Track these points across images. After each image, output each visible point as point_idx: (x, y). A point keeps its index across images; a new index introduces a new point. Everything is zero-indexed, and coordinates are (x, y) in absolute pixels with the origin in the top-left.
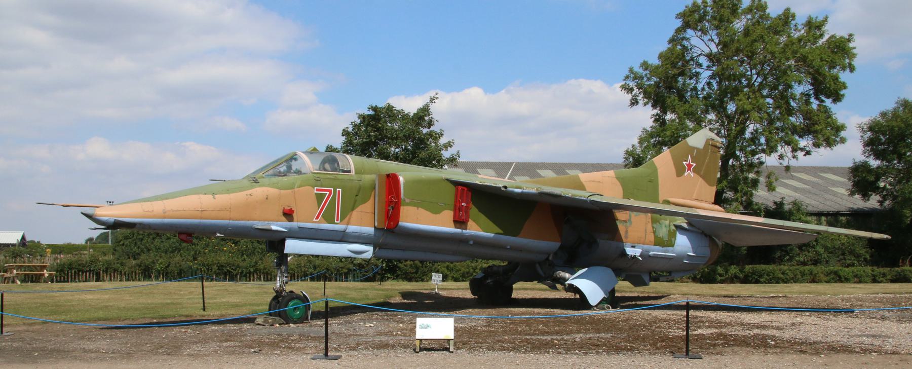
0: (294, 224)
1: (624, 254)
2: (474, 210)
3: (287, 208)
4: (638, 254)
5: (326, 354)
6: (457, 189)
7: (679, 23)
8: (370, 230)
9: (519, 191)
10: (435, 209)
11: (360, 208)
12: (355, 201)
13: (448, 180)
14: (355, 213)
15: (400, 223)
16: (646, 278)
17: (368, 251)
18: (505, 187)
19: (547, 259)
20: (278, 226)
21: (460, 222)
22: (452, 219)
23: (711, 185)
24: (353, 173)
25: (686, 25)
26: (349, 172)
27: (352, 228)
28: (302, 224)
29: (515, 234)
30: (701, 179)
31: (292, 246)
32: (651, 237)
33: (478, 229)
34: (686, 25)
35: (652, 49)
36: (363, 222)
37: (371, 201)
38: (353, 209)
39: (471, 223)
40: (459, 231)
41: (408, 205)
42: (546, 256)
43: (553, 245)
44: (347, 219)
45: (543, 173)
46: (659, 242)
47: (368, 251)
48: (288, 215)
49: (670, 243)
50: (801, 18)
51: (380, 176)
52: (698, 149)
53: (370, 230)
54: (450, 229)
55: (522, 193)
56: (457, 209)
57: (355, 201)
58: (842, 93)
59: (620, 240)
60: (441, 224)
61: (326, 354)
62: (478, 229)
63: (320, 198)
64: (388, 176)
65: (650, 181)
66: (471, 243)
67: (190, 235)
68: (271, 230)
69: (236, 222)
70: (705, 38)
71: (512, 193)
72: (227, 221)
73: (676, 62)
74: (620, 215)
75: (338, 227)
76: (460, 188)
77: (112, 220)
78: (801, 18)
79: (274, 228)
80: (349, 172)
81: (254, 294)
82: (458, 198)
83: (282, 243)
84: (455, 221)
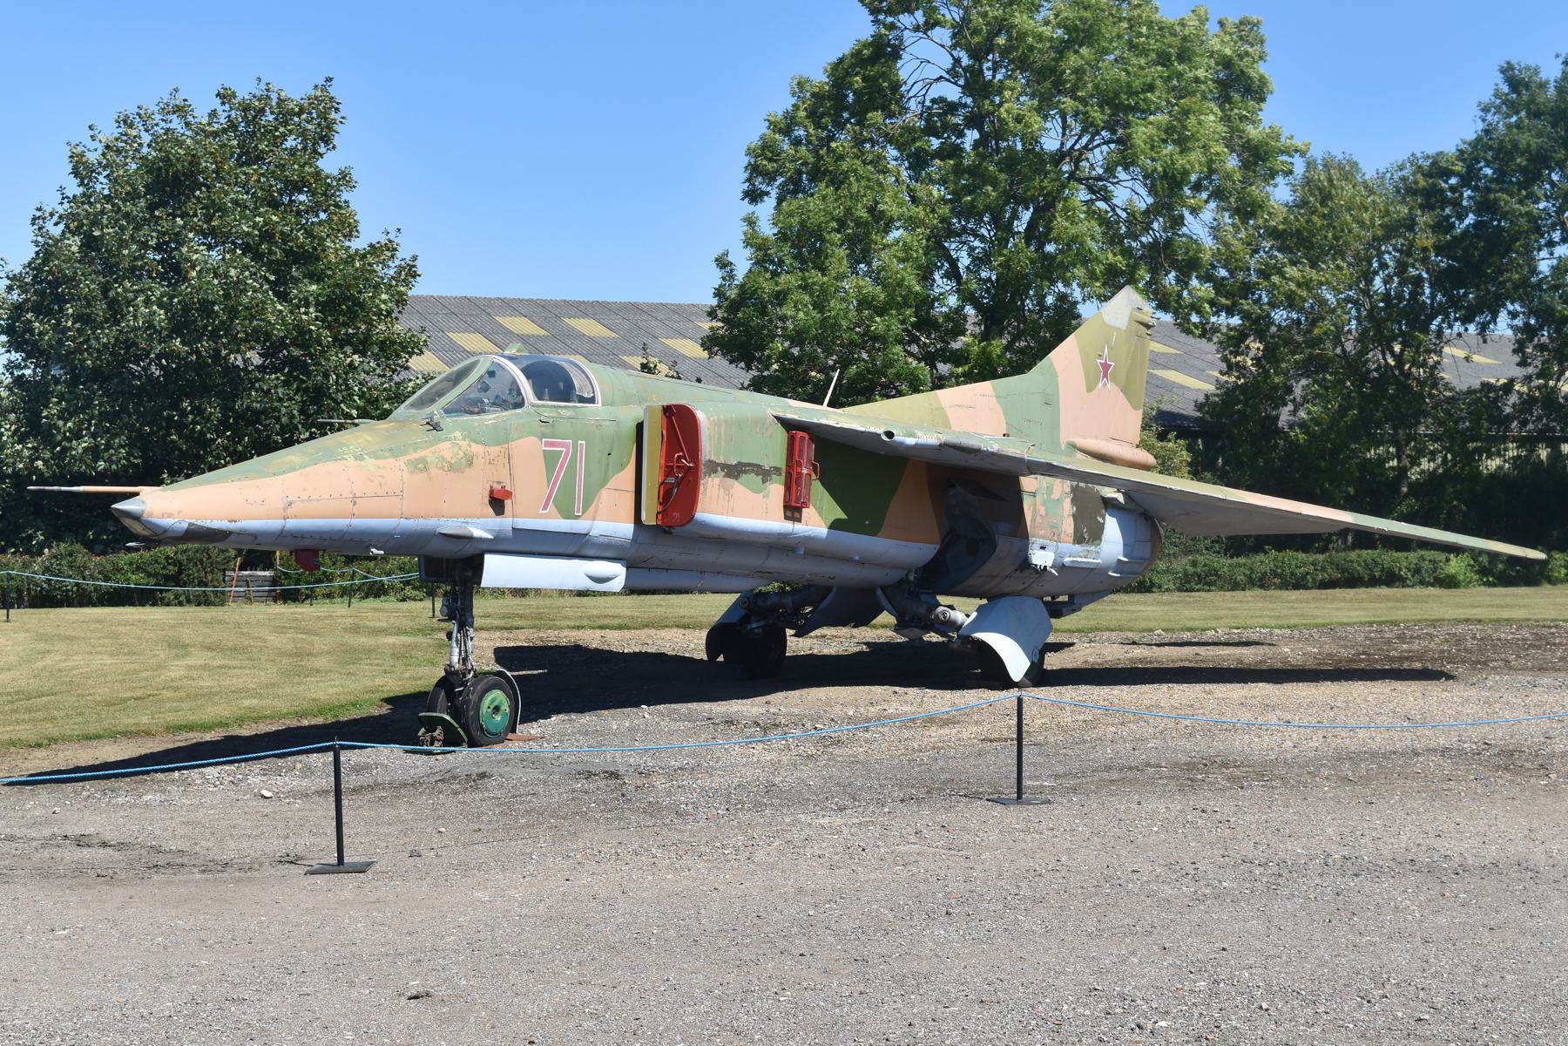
1: (1026, 564)
3: (497, 487)
4: (1049, 564)
5: (1019, 797)
14: (604, 493)
20: (481, 527)
21: (793, 510)
23: (1135, 408)
29: (873, 531)
38: (603, 485)
42: (902, 574)
44: (591, 509)
53: (624, 529)
55: (917, 447)
59: (1024, 536)
61: (1019, 797)
63: (550, 460)
67: (314, 552)
71: (902, 444)
74: (1028, 483)
83: (474, 565)
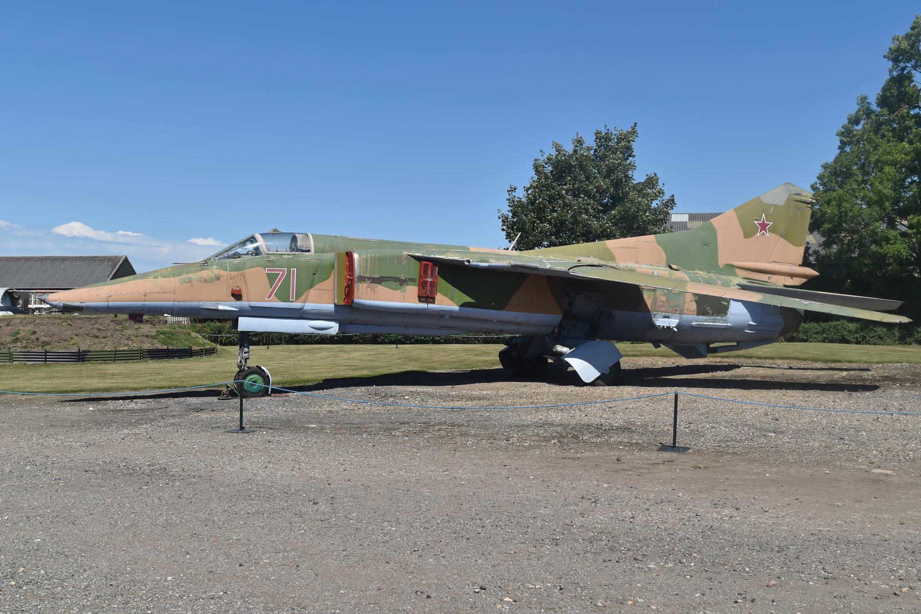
0: (244, 304)
1: (653, 325)
2: (442, 283)
8: (330, 307)
9: (486, 264)
13: (411, 256)
14: (312, 291)
17: (333, 328)
18: (469, 261)
19: (553, 332)
20: (227, 306)
24: (312, 252)
27: (309, 306)
29: (500, 307)
30: (781, 239)
31: (126, 316)
33: (447, 302)
36: (322, 298)
38: (311, 287)
39: (439, 297)
40: (424, 305)
43: (555, 318)
44: (303, 298)
47: (333, 328)
48: (237, 296)
51: (338, 255)
52: (776, 206)
53: (330, 307)
54: (415, 304)
56: (422, 285)
58: (638, 176)
59: (647, 310)
60: (406, 299)
62: (447, 302)
63: (272, 278)
64: (347, 253)
66: (447, 317)
68: (217, 310)
69: (182, 303)
72: (171, 303)
79: (221, 307)
80: (309, 251)
81: (224, 365)
82: (424, 271)
84: (420, 297)
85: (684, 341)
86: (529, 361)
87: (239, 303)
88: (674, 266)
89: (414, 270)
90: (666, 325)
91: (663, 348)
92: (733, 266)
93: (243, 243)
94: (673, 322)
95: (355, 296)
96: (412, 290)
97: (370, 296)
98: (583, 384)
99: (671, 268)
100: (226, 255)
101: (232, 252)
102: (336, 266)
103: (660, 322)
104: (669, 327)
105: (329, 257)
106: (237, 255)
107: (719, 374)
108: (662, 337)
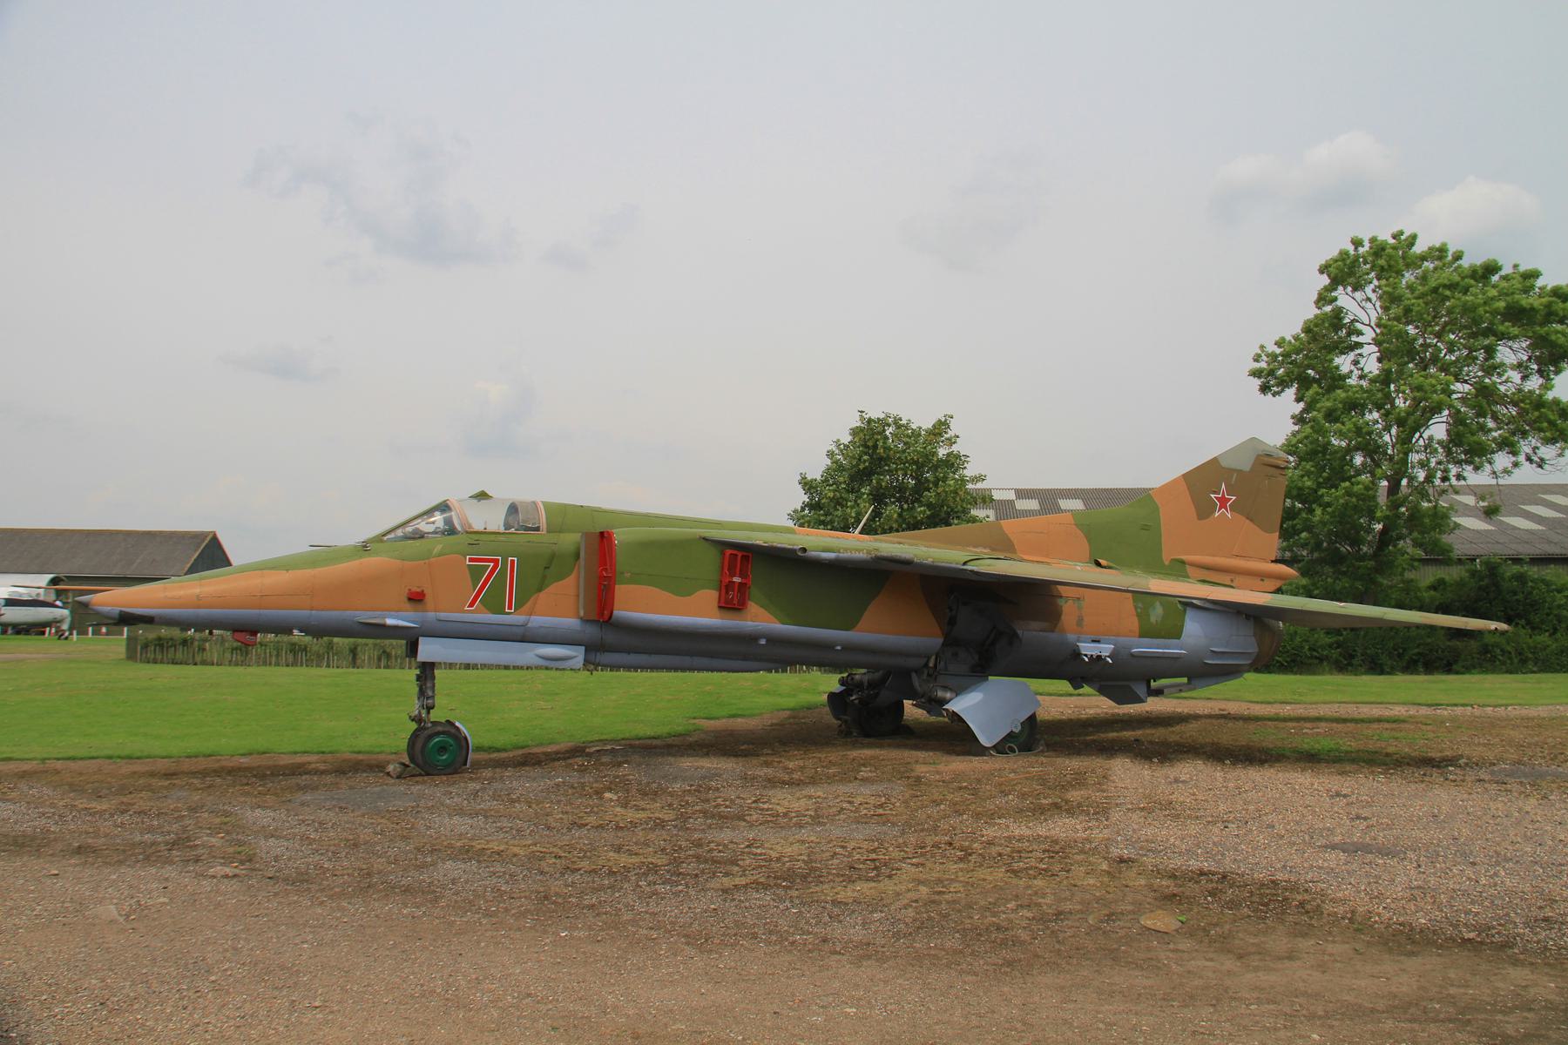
3: (415, 589)
6: (723, 554)
7: (1325, 280)
9: (832, 555)
10: (680, 586)
11: (553, 589)
12: (545, 577)
15: (616, 613)
16: (1140, 690)
18: (804, 550)
22: (715, 604)
25: (1336, 282)
26: (538, 529)
27: (539, 621)
28: (443, 615)
32: (1134, 624)
33: (759, 619)
34: (1336, 282)
35: (1289, 314)
37: (570, 581)
38: (540, 590)
39: (753, 608)
41: (636, 579)
45: (1065, 504)
46: (1147, 632)
48: (416, 598)
49: (1176, 633)
50: (1451, 250)
51: (587, 535)
52: (1239, 472)
54: (336, 640)
56: (725, 588)
57: (545, 577)
60: (699, 612)
64: (602, 534)
65: (1145, 528)
70: (1358, 295)
72: (306, 613)
73: (1327, 333)
75: (513, 618)
76: (729, 552)
77: (116, 610)
78: (1451, 250)
79: (390, 622)
80: (538, 529)
85: (1119, 678)
86: (874, 712)
87: (418, 615)
88: (1103, 562)
89: (710, 563)
90: (1095, 653)
91: (1086, 689)
92: (1183, 562)
93: (429, 512)
94: (1105, 649)
95: (616, 603)
96: (710, 596)
97: (640, 605)
98: (981, 751)
99: (1098, 564)
100: (399, 533)
101: (409, 529)
102: (582, 554)
103: (1088, 649)
104: (1099, 657)
105: (570, 540)
106: (419, 535)
107: (1158, 734)
108: (1078, 671)
